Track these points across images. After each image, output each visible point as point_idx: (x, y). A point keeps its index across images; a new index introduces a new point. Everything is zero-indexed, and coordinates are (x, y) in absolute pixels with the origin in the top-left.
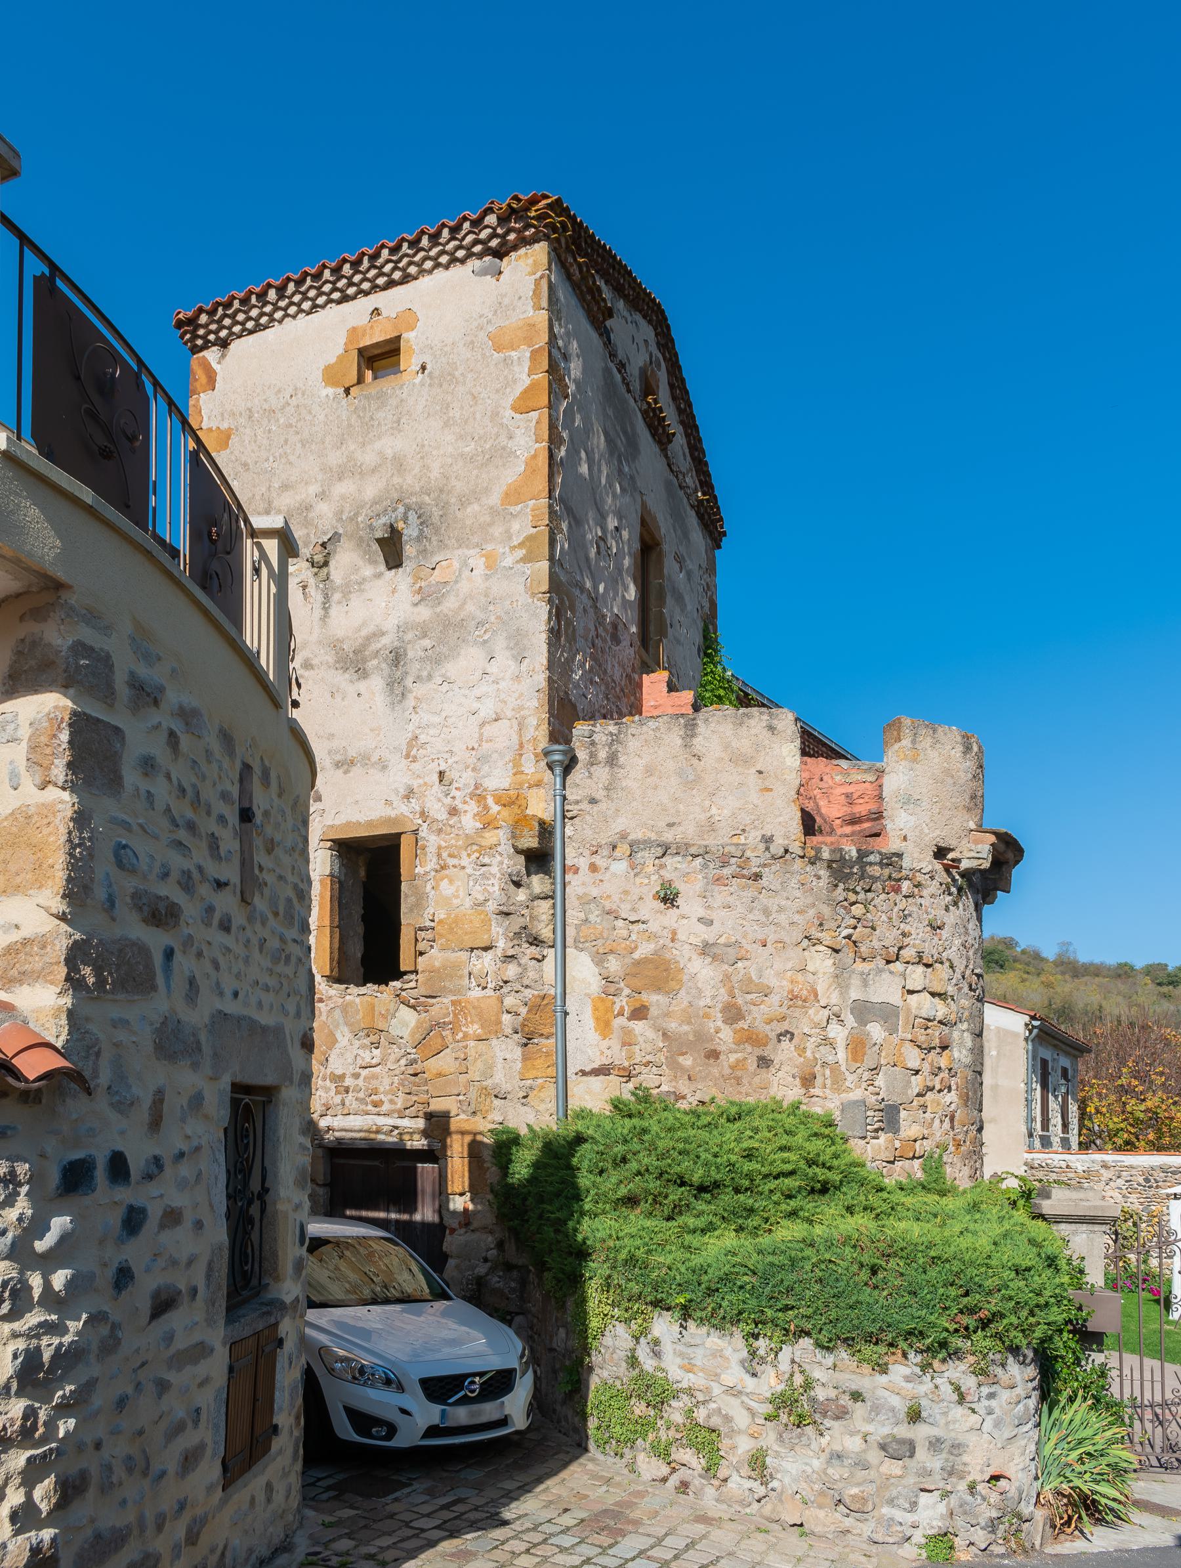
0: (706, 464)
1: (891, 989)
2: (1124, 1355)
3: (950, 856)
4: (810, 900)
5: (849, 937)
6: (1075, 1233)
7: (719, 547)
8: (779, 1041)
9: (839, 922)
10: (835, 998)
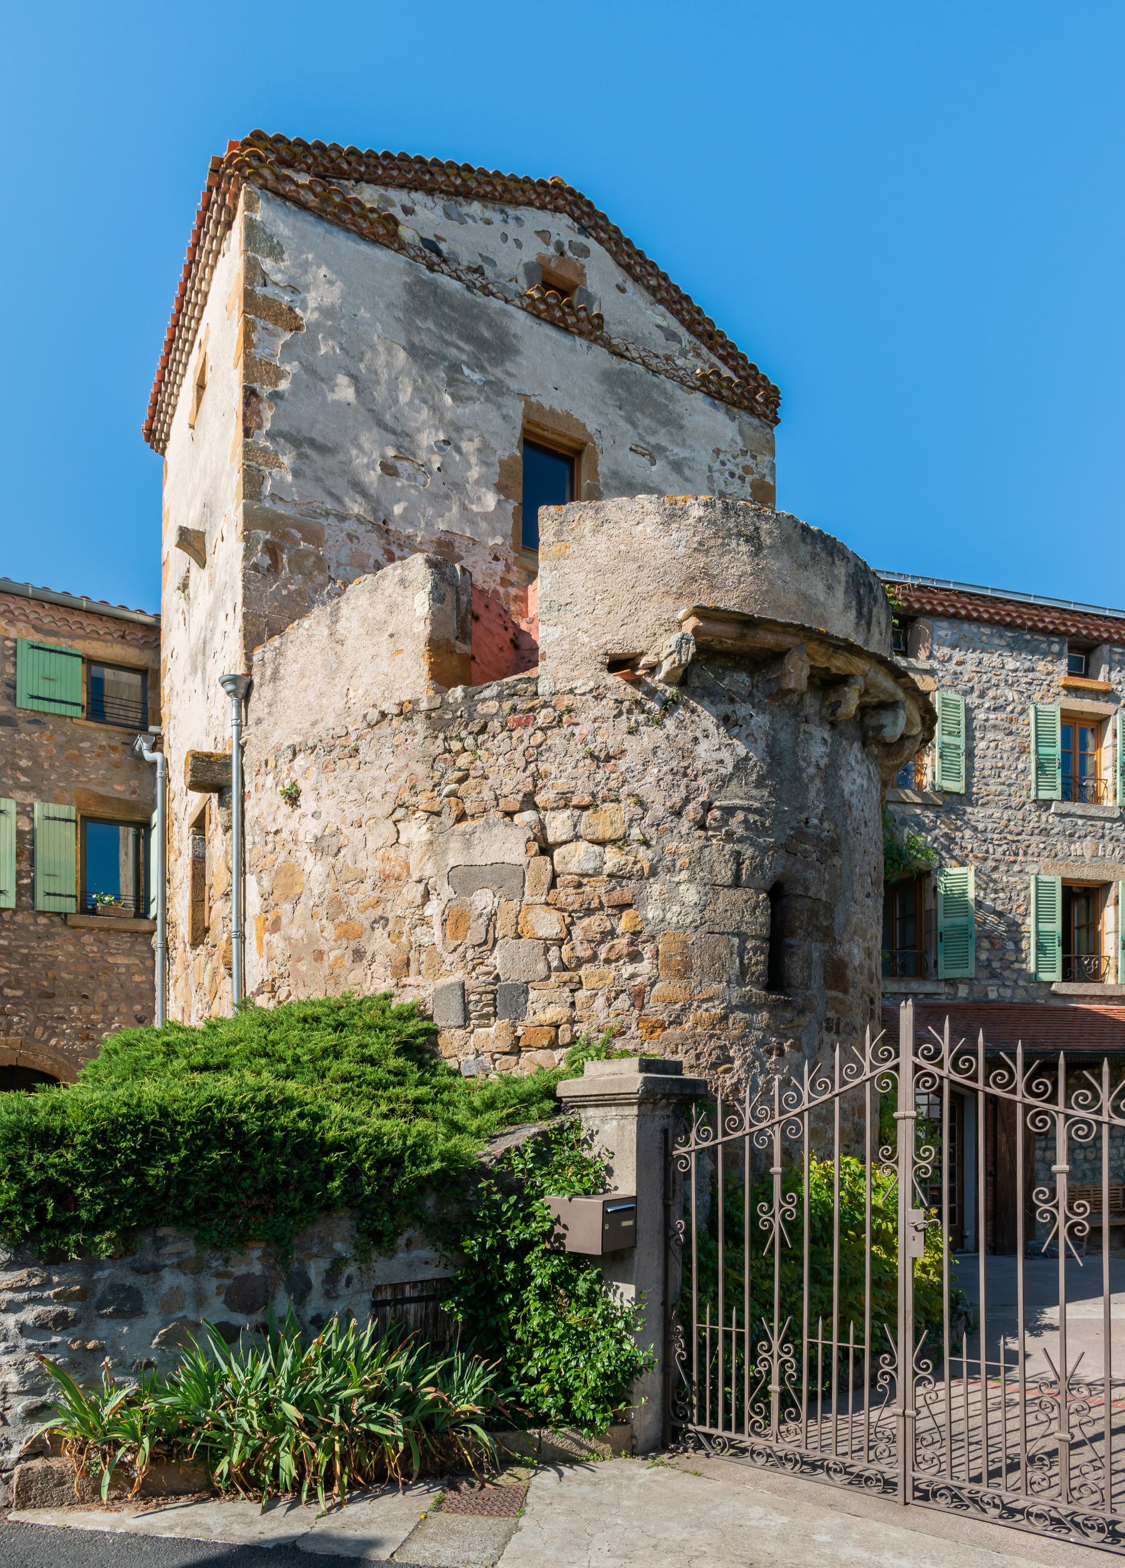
0: (722, 335)
1: (508, 845)
2: (1046, 1321)
3: (643, 661)
4: (403, 762)
5: (453, 794)
6: (604, 1120)
7: (777, 421)
8: (373, 929)
9: (436, 780)
10: (429, 870)
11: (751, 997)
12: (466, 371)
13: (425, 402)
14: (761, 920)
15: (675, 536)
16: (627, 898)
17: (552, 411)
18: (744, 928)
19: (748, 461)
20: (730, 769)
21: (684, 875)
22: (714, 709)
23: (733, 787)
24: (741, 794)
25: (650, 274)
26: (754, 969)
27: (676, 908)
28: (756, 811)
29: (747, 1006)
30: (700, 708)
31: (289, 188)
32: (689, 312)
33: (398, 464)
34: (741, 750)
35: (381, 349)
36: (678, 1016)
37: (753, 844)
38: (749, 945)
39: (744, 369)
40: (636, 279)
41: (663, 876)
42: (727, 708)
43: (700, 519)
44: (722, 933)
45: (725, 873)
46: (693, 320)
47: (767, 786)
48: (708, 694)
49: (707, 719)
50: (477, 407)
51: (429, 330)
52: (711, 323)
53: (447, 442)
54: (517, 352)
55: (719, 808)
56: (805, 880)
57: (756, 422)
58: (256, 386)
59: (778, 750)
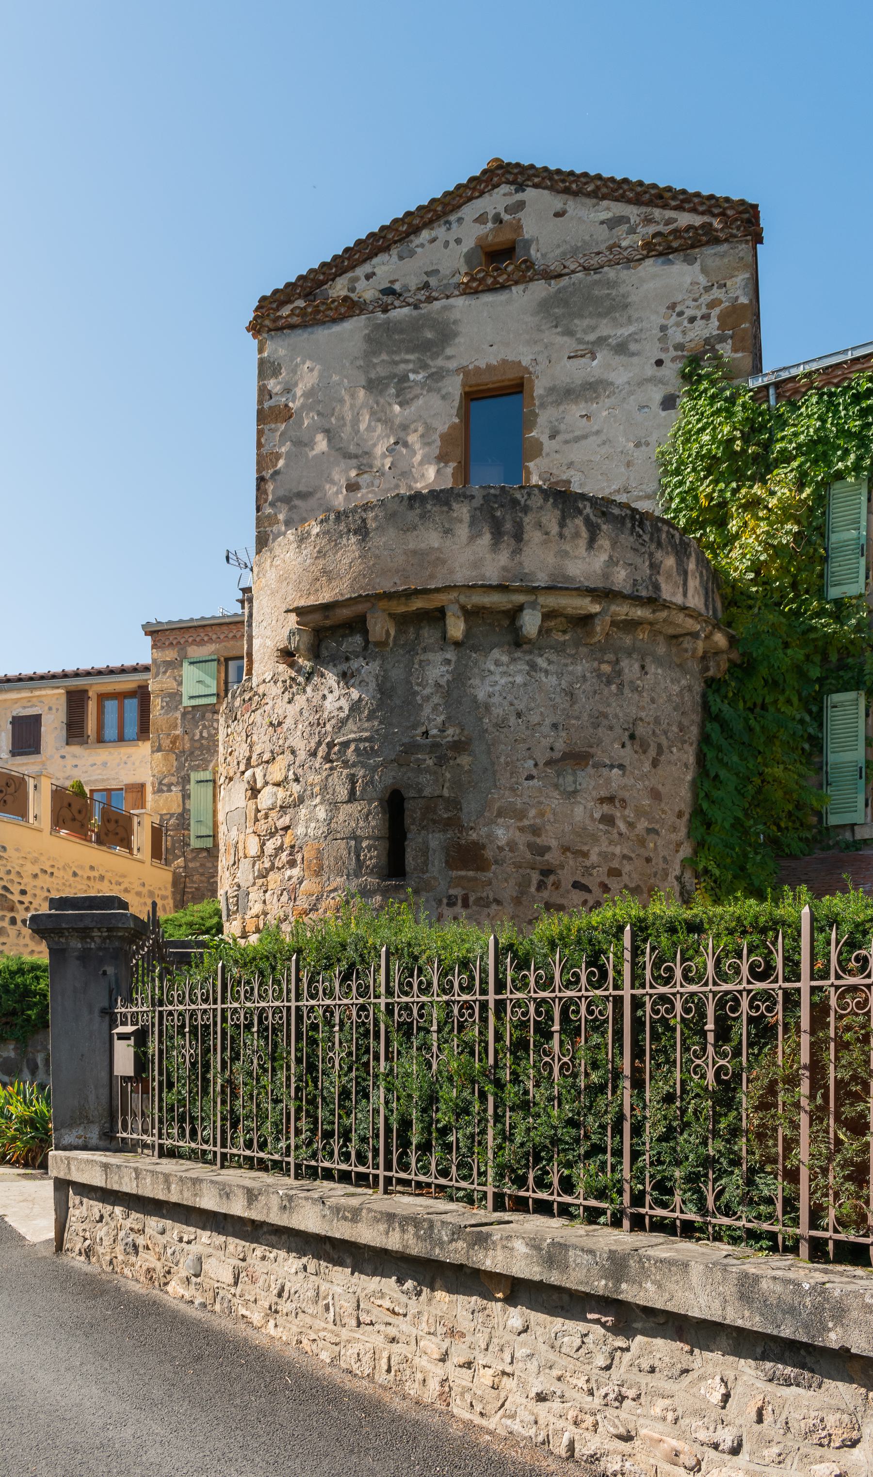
0: (669, 189)
11: (366, 885)
12: (412, 376)
13: (379, 420)
14: (373, 823)
15: (305, 552)
16: (287, 823)
17: (489, 367)
18: (359, 832)
19: (716, 293)
20: (347, 712)
21: (318, 800)
22: (335, 670)
23: (350, 725)
24: (355, 729)
25: (586, 184)
26: (368, 863)
27: (313, 825)
28: (366, 740)
29: (365, 893)
30: (326, 672)
31: (281, 323)
32: (632, 190)
33: (359, 480)
34: (355, 694)
35: (347, 398)
36: (315, 905)
37: (364, 765)
38: (364, 845)
39: (702, 204)
40: (575, 194)
41: (307, 802)
42: (344, 667)
43: (317, 534)
44: (343, 839)
45: (343, 793)
46: (638, 194)
47: (377, 717)
48: (332, 661)
49: (331, 679)
50: (420, 401)
51: (383, 361)
52: (654, 186)
53: (396, 443)
54: (455, 335)
55: (339, 744)
56: (418, 784)
57: (725, 247)
58: (264, 473)
59: (388, 685)
